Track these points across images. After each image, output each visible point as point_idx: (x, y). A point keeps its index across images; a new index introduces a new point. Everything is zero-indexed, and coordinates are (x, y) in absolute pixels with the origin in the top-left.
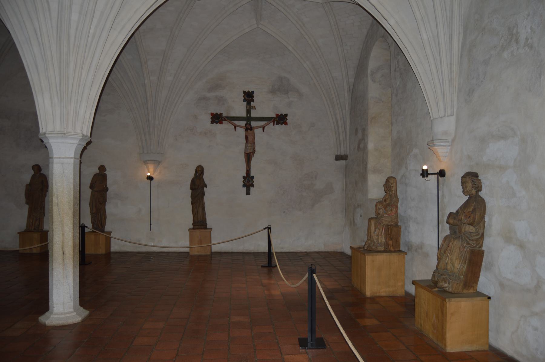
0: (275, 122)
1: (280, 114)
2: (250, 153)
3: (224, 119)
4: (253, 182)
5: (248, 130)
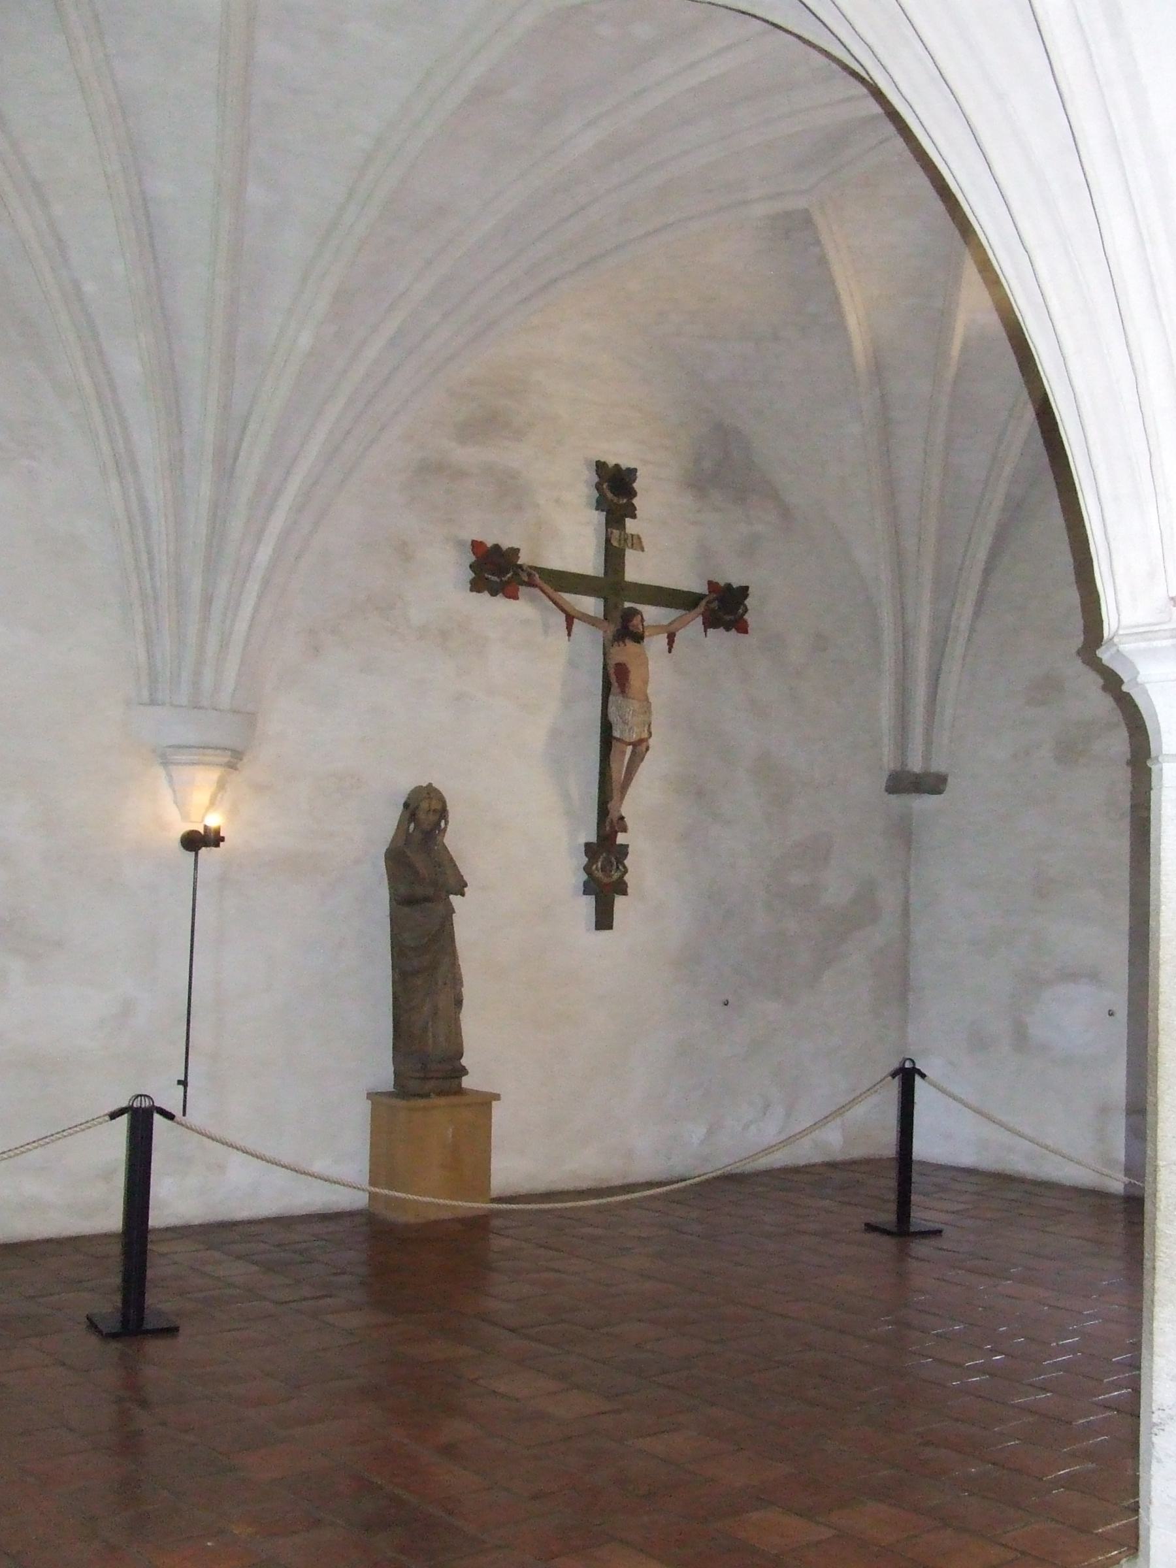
3: (526, 579)
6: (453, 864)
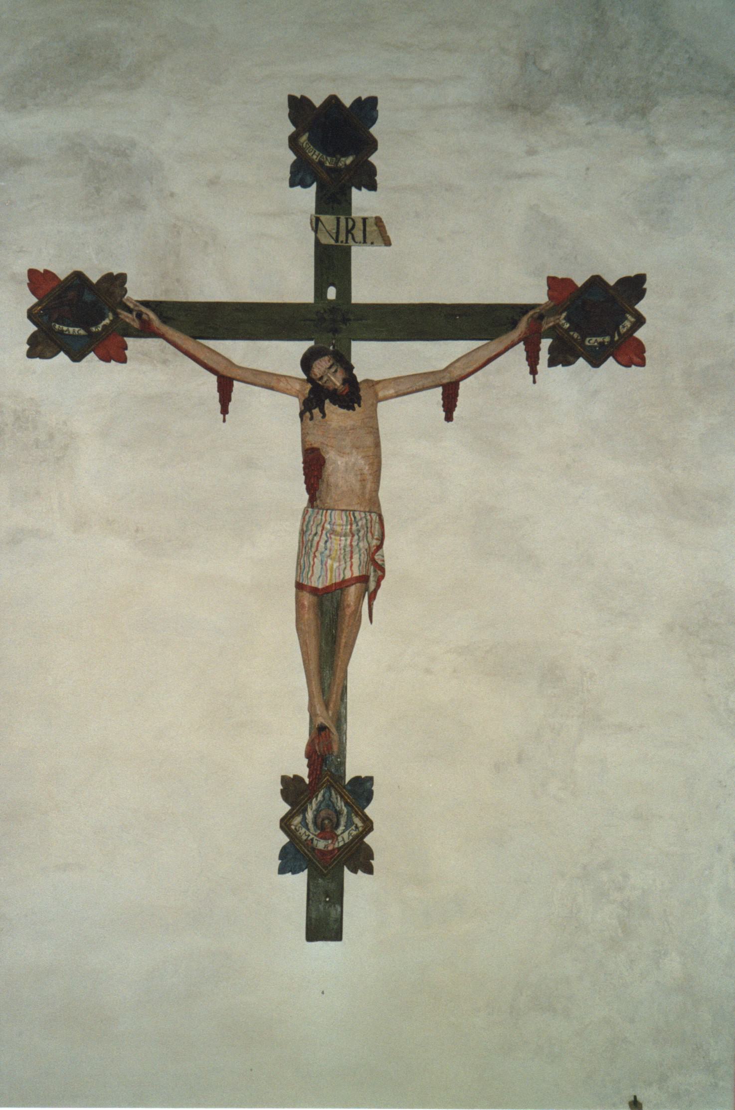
0: (546, 344)
1: (580, 282)
2: (343, 585)
3: (136, 324)
4: (368, 826)
5: (328, 406)
6: (303, 431)
